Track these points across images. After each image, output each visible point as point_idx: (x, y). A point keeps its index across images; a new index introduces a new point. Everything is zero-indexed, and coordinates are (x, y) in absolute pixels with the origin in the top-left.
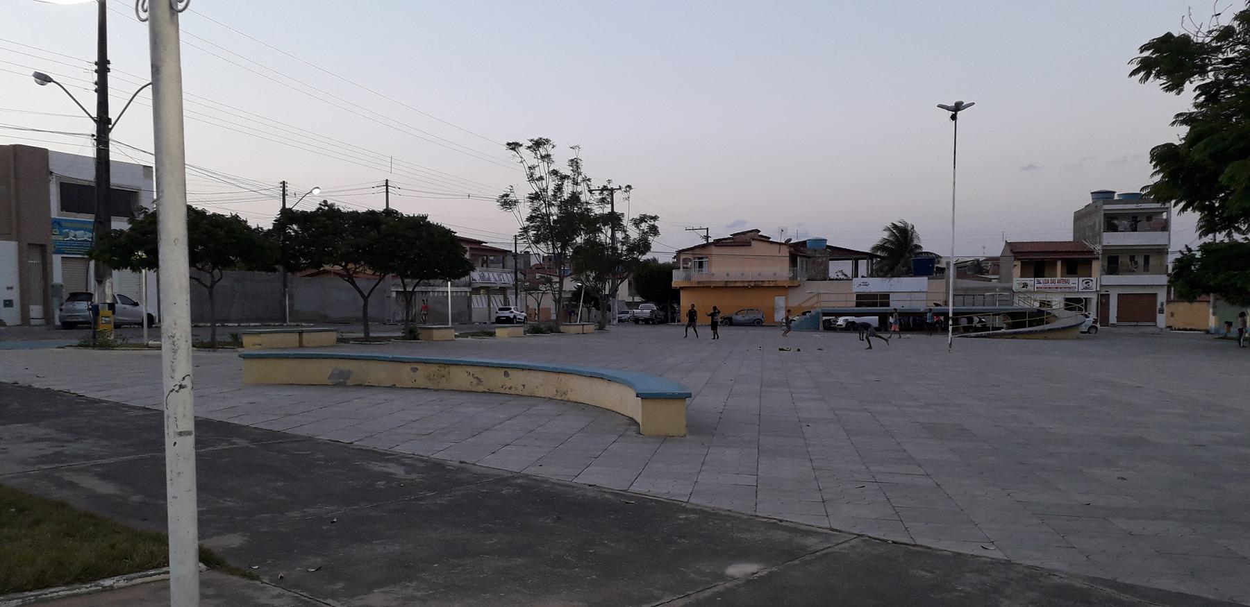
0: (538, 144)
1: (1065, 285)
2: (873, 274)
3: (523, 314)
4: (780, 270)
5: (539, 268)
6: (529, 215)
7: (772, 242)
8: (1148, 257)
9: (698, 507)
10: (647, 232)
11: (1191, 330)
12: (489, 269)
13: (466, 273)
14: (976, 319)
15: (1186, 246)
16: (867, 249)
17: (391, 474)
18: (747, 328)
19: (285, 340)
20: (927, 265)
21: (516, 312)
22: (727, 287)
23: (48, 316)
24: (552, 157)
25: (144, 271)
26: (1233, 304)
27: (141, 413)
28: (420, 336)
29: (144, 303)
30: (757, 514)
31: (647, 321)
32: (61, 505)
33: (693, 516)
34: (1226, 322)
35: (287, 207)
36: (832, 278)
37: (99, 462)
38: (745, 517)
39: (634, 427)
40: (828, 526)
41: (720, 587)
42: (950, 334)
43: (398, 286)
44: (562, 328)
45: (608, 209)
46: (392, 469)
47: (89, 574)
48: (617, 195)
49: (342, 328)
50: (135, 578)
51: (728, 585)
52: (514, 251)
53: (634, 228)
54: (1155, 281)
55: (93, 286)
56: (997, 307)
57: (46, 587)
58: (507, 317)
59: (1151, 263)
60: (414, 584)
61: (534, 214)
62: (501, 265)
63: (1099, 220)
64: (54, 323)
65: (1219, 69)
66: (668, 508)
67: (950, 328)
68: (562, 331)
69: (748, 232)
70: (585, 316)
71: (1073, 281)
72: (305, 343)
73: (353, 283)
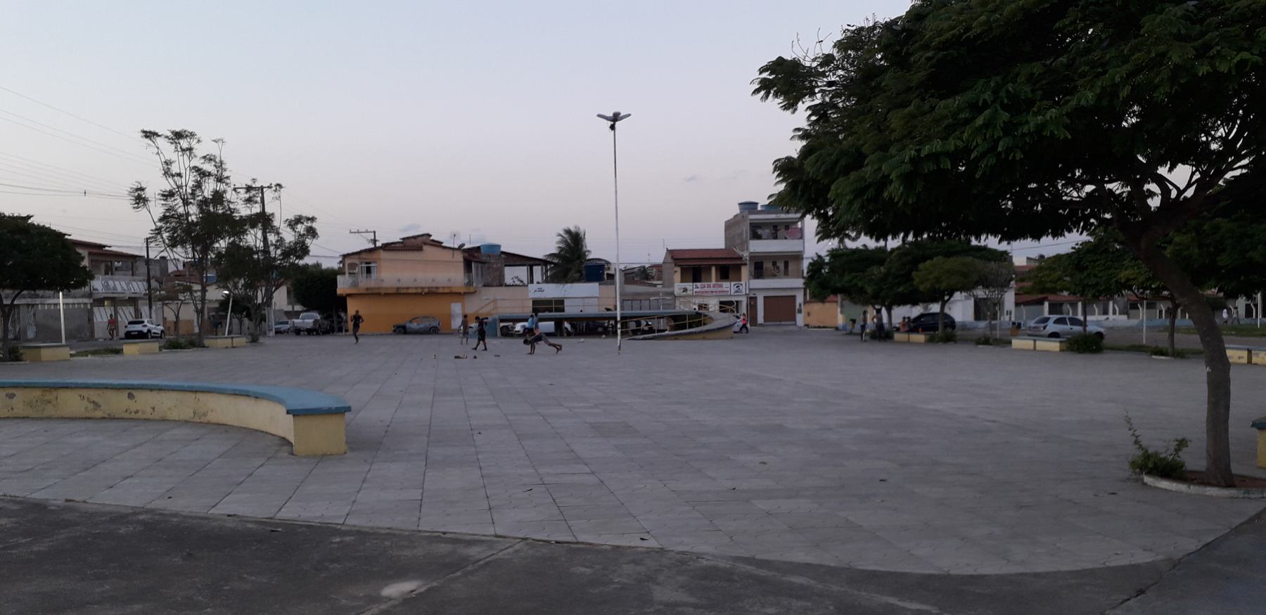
0: (178, 135)
1: (719, 289)
2: (548, 280)
3: (159, 327)
4: (455, 276)
5: (178, 275)
6: (161, 215)
7: (445, 248)
8: (787, 262)
10: (304, 234)
11: (824, 327)
12: (114, 277)
13: (83, 283)
14: (644, 323)
15: (817, 254)
16: (540, 255)
18: (422, 336)
20: (597, 272)
21: (150, 324)
22: (399, 294)
24: (194, 151)
26: (856, 303)
28: (24, 356)
30: (420, 529)
31: (310, 332)
33: (347, 539)
34: (852, 320)
36: (508, 283)
38: (407, 533)
39: (286, 448)
40: (493, 533)
42: (619, 337)
44: (207, 342)
45: (256, 209)
48: (268, 195)
51: (383, 607)
53: (289, 229)
54: (793, 284)
56: (661, 310)
58: (138, 331)
59: (790, 268)
61: (168, 214)
62: (131, 272)
63: (746, 228)
65: (825, 91)
66: (321, 532)
67: (619, 331)
68: (206, 345)
69: (419, 236)
70: (236, 327)
71: (726, 285)
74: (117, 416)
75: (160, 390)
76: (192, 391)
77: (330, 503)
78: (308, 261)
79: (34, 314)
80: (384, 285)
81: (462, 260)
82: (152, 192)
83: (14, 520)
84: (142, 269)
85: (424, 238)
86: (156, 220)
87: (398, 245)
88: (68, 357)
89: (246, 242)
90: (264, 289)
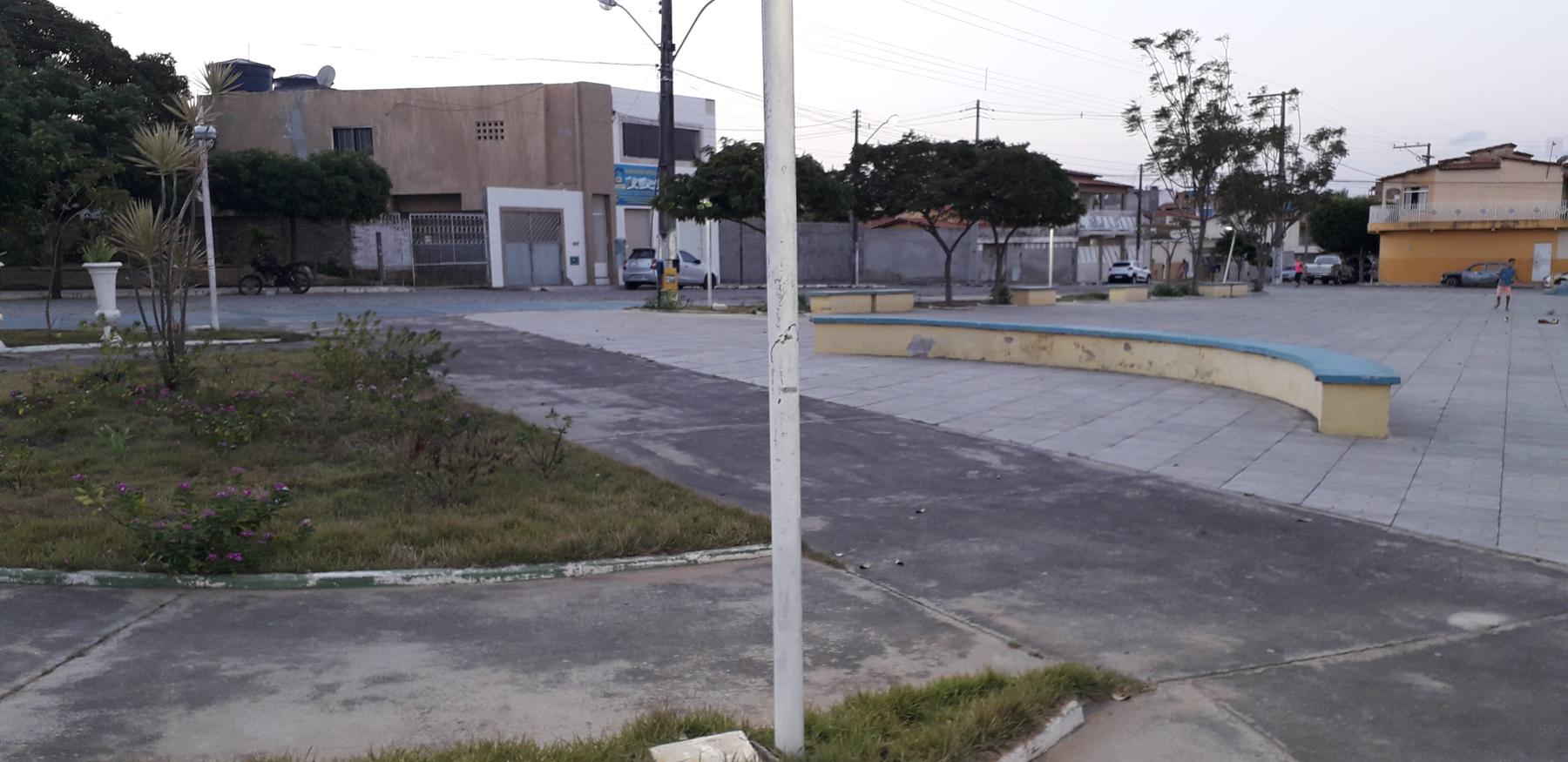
0: (1171, 40)
5: (1169, 209)
9: (1407, 534)
17: (985, 463)
18: (1485, 290)
19: (856, 303)
21: (1137, 268)
22: (1456, 230)
23: (612, 275)
25: (708, 222)
27: (710, 381)
29: (708, 260)
30: (1501, 548)
31: (1325, 280)
32: (643, 472)
33: (1397, 545)
35: (862, 142)
37: (673, 431)
38: (1481, 551)
39: (1308, 423)
41: (1440, 639)
43: (985, 236)
44: (1201, 289)
46: (986, 457)
47: (673, 546)
49: (919, 290)
50: (718, 554)
51: (1454, 638)
52: (1137, 187)
55: (656, 243)
57: (635, 555)
60: (1019, 592)
64: (618, 282)
66: (1363, 532)
68: (1201, 293)
70: (1234, 273)
72: (878, 308)
73: (935, 234)
74: (1111, 369)
75: (1160, 342)
76: (1196, 346)
77: (1372, 497)
78: (1333, 186)
79: (1021, 255)
80: (1435, 218)
81: (1562, 180)
82: (1147, 113)
83: (1021, 467)
84: (1132, 201)
85: (1504, 150)
86: (1152, 143)
87: (1462, 162)
88: (1054, 301)
89: (1256, 166)
90: (1274, 224)
